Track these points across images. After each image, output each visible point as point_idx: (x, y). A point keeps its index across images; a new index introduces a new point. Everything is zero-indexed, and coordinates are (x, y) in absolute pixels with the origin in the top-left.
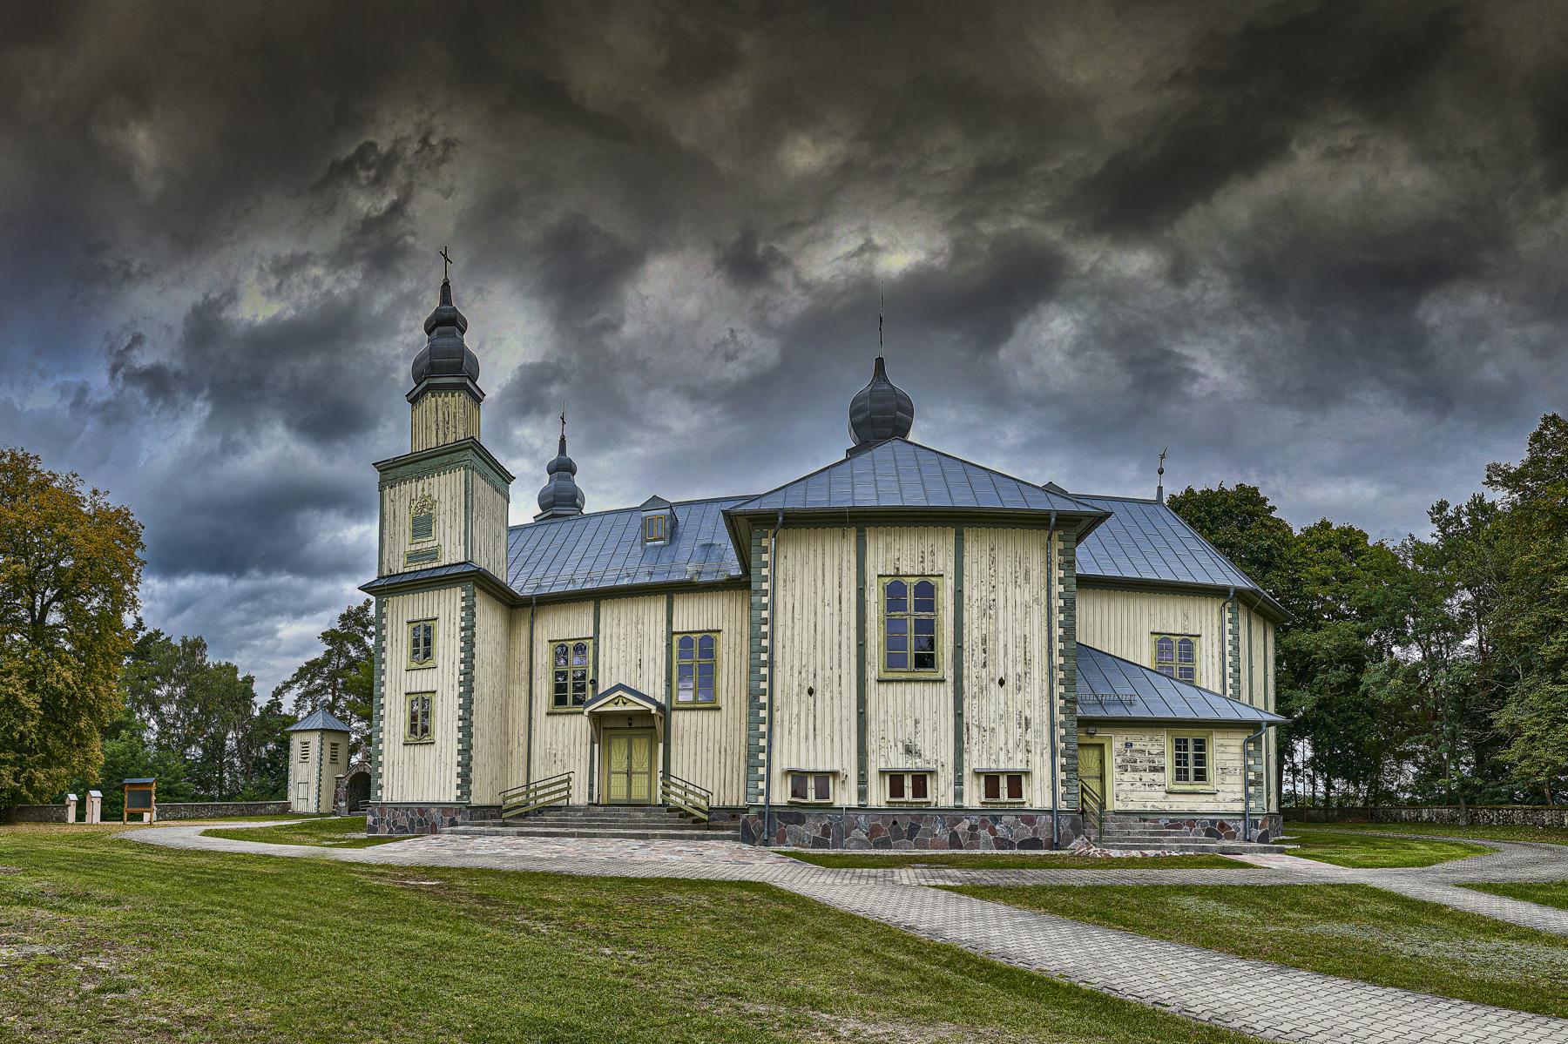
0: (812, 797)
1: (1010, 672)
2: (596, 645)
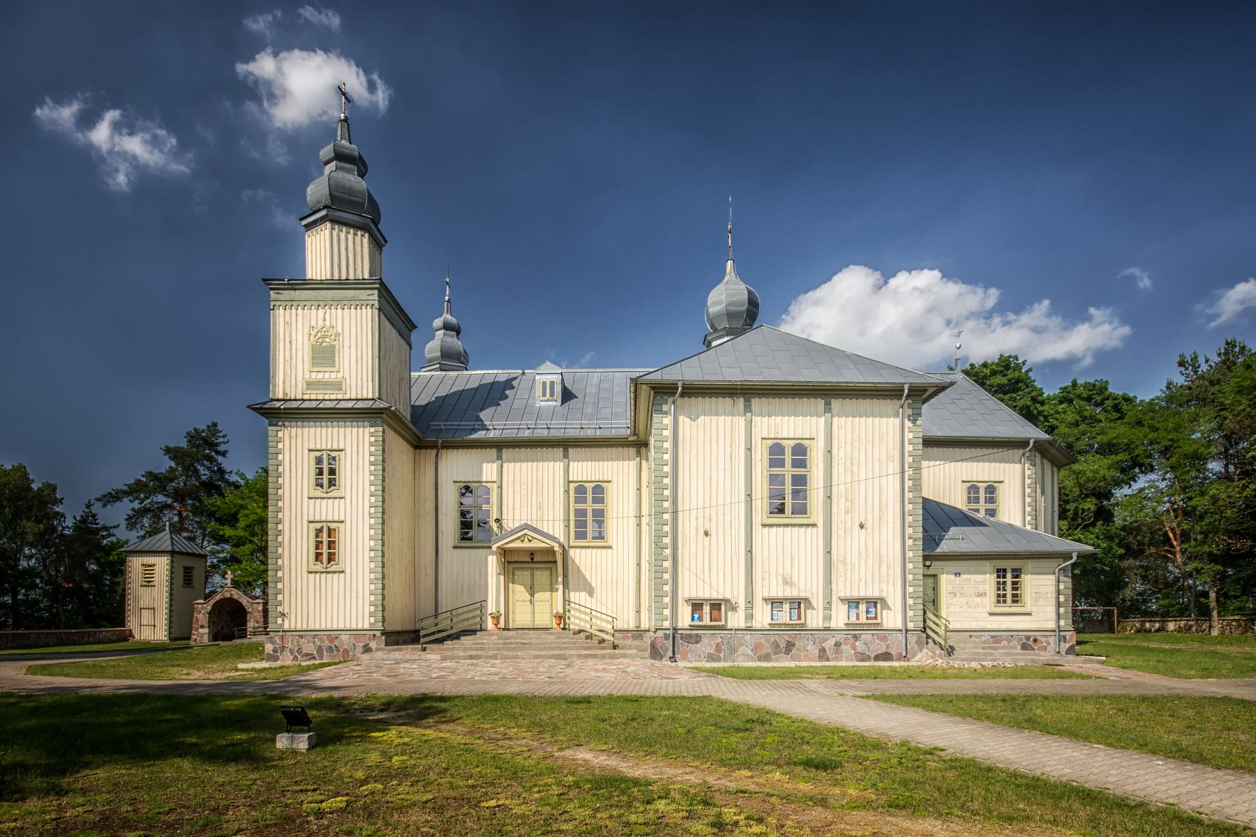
0: (707, 621)
1: (870, 518)
2: (500, 487)
